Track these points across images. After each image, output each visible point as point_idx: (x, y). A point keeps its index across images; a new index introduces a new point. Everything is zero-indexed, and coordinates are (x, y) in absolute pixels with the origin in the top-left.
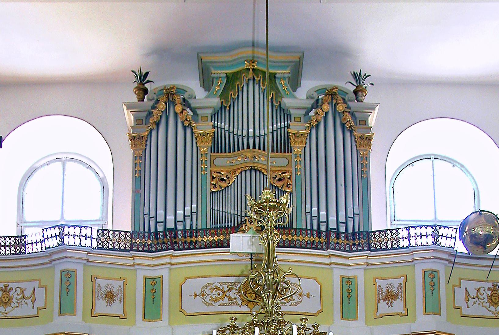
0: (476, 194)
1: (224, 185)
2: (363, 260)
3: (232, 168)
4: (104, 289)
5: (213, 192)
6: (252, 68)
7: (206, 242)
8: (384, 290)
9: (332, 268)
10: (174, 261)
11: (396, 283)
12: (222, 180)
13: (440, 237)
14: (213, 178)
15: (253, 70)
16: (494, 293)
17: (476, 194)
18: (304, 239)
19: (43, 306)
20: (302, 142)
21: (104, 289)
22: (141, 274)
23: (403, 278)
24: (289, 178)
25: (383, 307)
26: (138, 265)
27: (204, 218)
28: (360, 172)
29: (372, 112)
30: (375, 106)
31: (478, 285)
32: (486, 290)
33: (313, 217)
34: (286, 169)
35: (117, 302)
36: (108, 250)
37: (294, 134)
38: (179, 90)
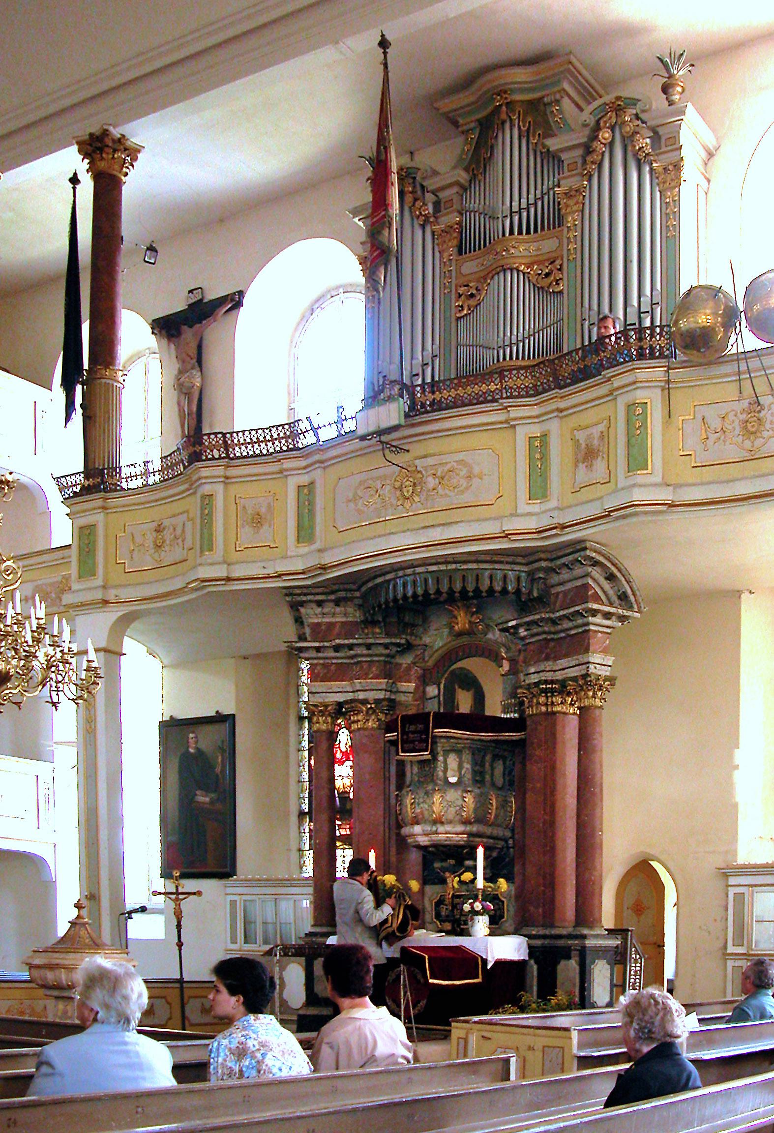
0: (293, 393)
1: (472, 302)
2: (99, 503)
3: (482, 274)
4: (250, 511)
5: (459, 318)
6: (505, 101)
7: (462, 397)
8: (583, 446)
9: (514, 426)
10: (562, 405)
11: (596, 431)
12: (472, 296)
13: (301, 436)
14: (460, 296)
15: (508, 104)
16: (751, 417)
17: (293, 393)
18: (457, 394)
19: (191, 546)
20: (577, 203)
21: (250, 511)
22: (293, 482)
23: (605, 422)
24: (560, 270)
25: (582, 475)
26: (287, 470)
27: (572, 325)
28: (664, 228)
29: (682, 120)
30: (683, 107)
31: (724, 408)
32: (739, 414)
33: (643, 313)
34: (554, 255)
35: (266, 527)
36: (255, 457)
37: (566, 194)
38: (410, 171)
